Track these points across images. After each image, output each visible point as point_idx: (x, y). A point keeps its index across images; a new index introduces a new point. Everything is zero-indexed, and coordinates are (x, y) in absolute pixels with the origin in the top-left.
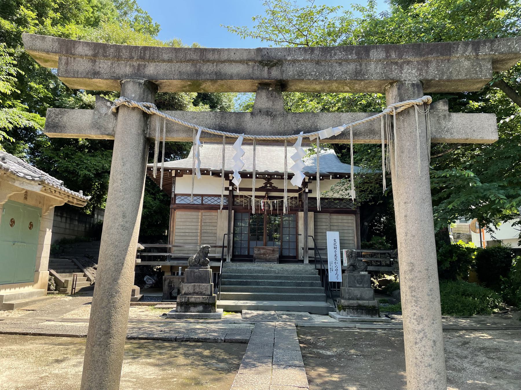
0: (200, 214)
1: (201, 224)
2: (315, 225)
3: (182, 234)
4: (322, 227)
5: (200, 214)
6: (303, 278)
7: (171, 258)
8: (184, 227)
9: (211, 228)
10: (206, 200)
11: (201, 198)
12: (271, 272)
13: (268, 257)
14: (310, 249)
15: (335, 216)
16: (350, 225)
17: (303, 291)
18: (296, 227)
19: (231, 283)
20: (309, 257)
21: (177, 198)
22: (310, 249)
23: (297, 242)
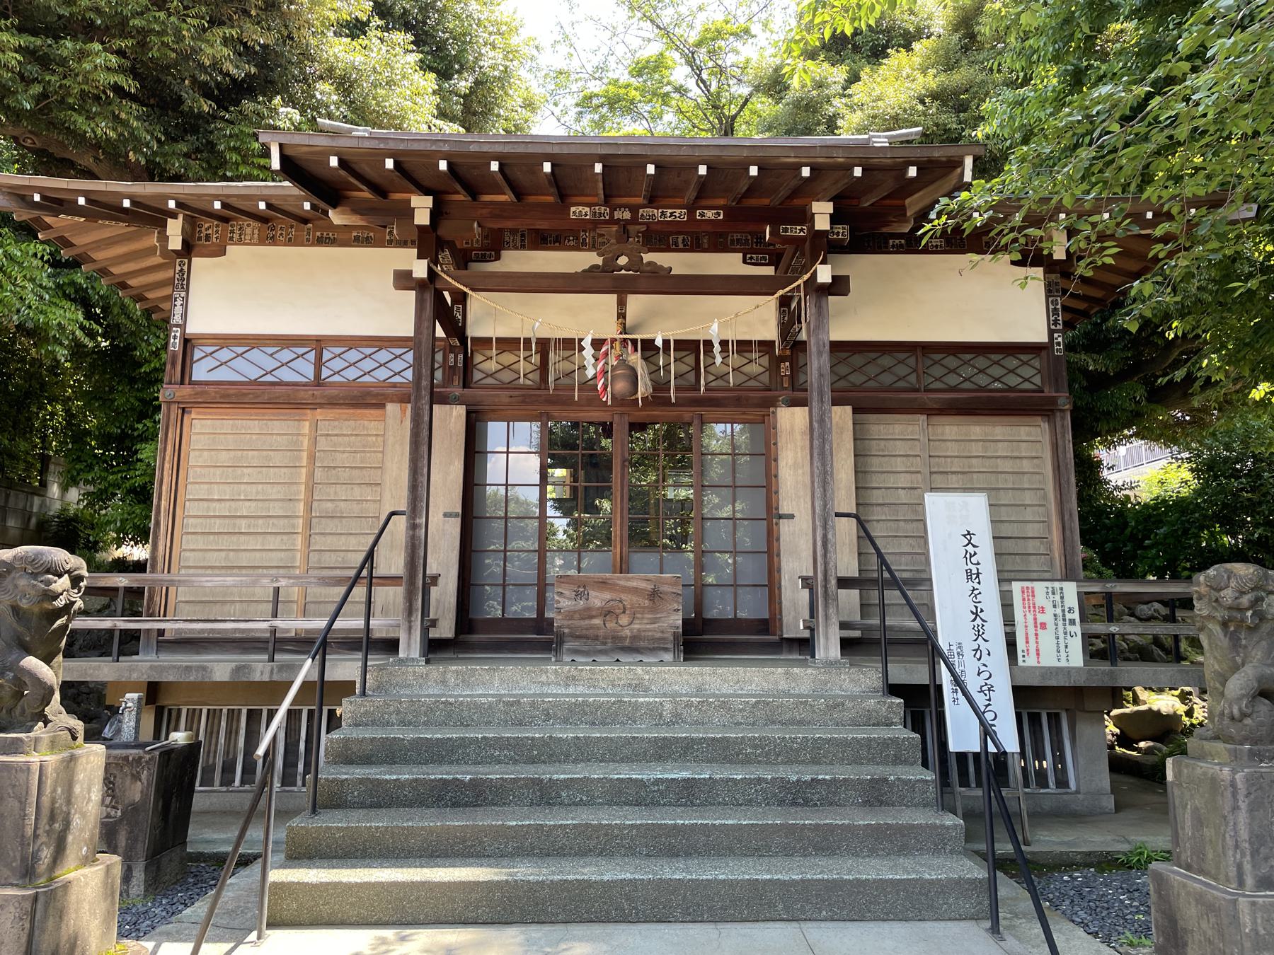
0: (306, 427)
1: (311, 475)
2: (860, 472)
3: (217, 526)
4: (891, 481)
5: (306, 427)
6: (817, 752)
7: (165, 643)
8: (228, 492)
9: (357, 493)
10: (337, 364)
11: (311, 356)
12: (630, 714)
13: (626, 626)
14: (844, 583)
15: (951, 429)
16: (1026, 466)
17: (825, 843)
18: (769, 486)
19: (380, 798)
20: (844, 626)
21: (197, 354)
22: (844, 583)
23: (771, 552)
